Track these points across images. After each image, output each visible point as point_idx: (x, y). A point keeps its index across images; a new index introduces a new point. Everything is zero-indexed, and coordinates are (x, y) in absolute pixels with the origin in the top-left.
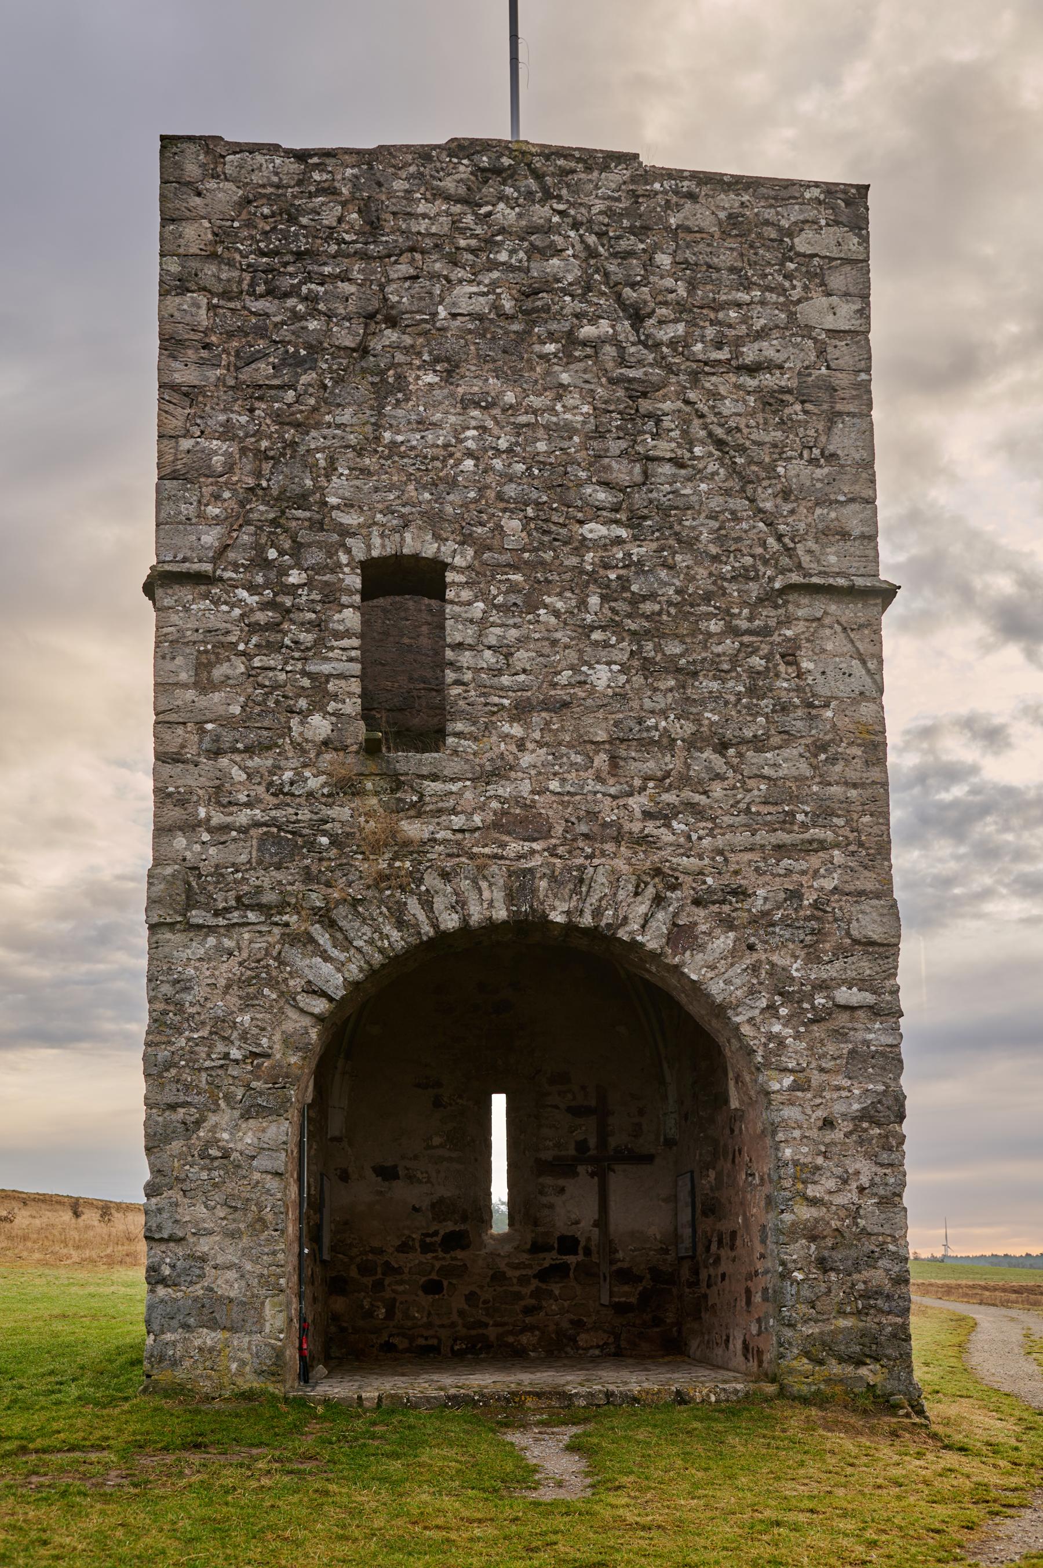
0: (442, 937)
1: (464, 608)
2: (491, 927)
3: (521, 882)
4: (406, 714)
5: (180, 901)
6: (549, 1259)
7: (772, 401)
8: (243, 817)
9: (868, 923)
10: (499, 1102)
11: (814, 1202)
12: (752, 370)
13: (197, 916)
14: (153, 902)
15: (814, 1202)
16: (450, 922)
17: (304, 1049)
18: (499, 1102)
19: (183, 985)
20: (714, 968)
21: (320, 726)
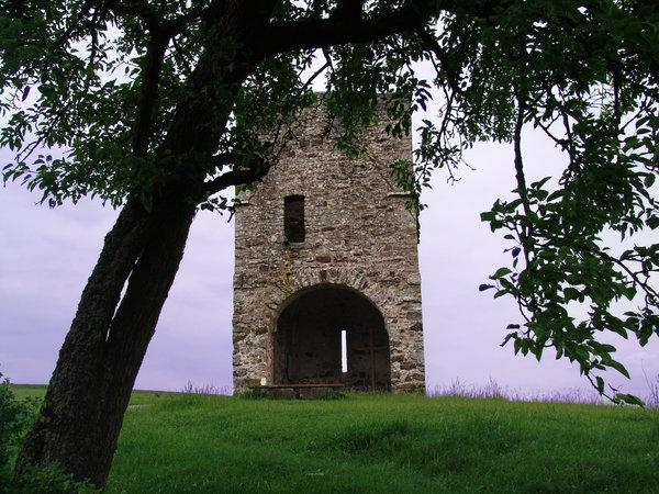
0: (304, 289)
1: (308, 207)
2: (316, 285)
3: (323, 274)
4: (295, 230)
5: (241, 283)
6: (358, 379)
7: (387, 148)
8: (255, 261)
9: (412, 279)
10: (344, 333)
11: (399, 352)
12: (382, 141)
13: (245, 286)
14: (235, 283)
15: (399, 352)
16: (306, 284)
17: (437, 393)
18: (344, 333)
19: (241, 303)
20: (372, 292)
21: (274, 238)
